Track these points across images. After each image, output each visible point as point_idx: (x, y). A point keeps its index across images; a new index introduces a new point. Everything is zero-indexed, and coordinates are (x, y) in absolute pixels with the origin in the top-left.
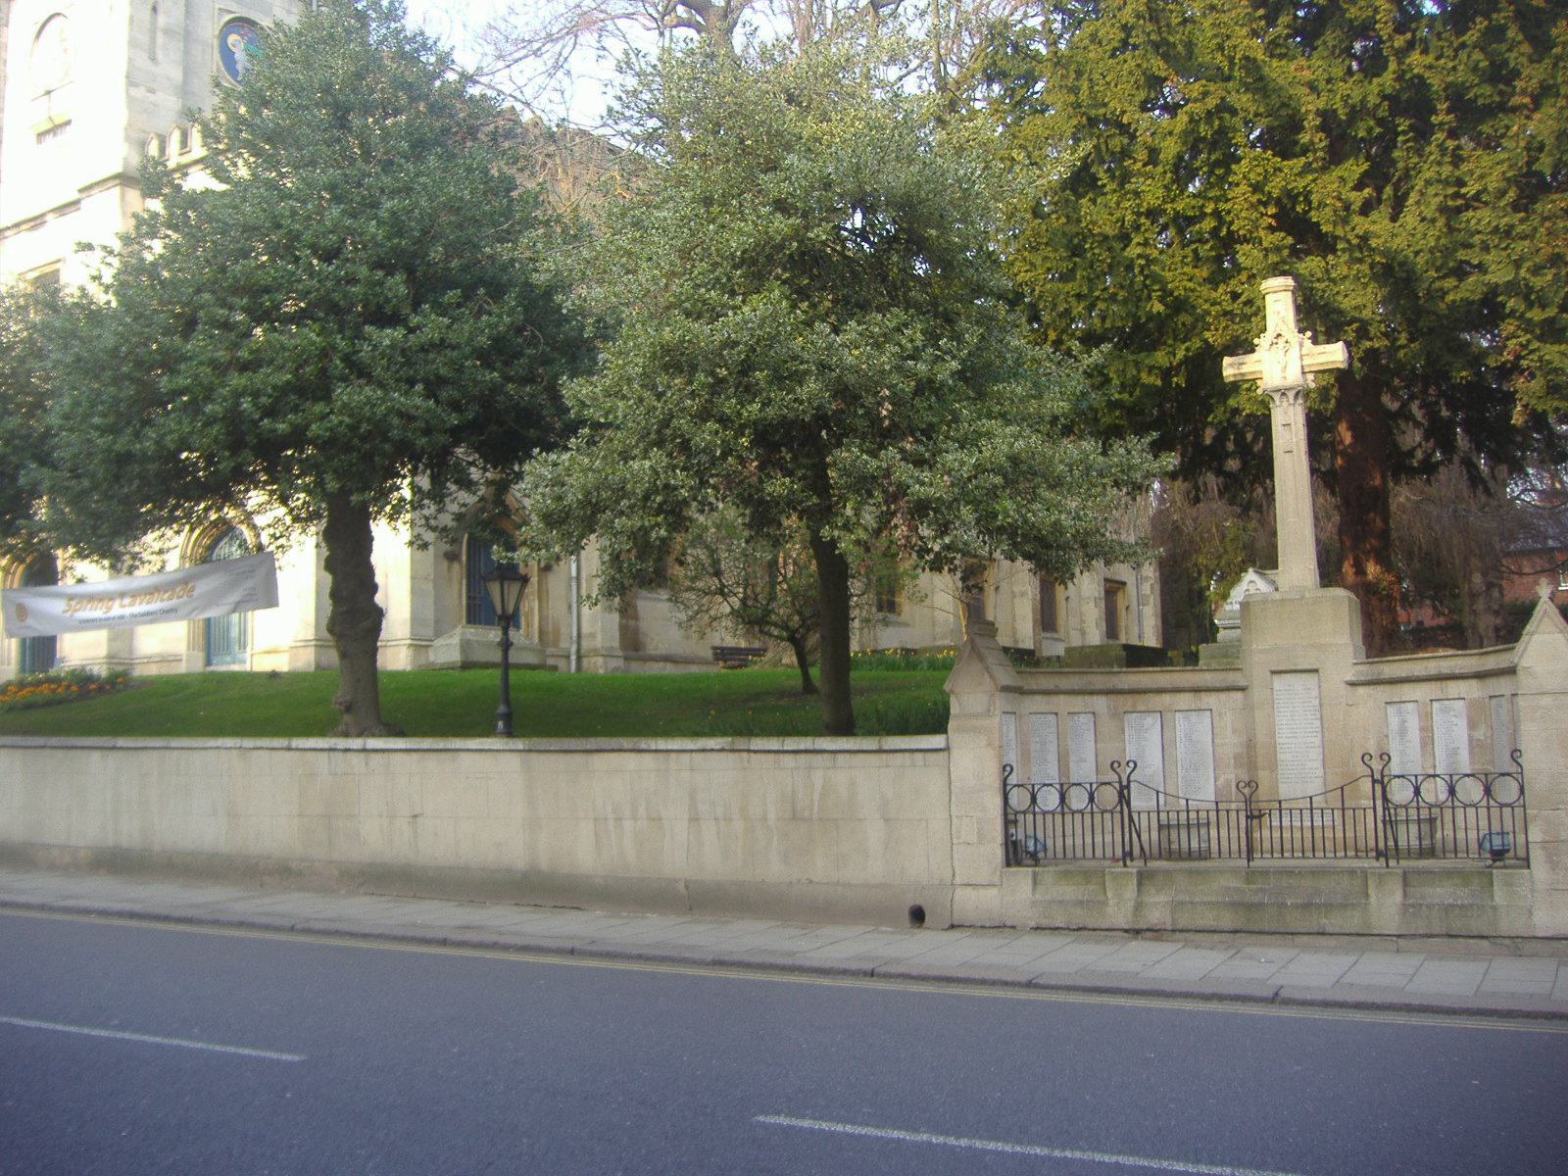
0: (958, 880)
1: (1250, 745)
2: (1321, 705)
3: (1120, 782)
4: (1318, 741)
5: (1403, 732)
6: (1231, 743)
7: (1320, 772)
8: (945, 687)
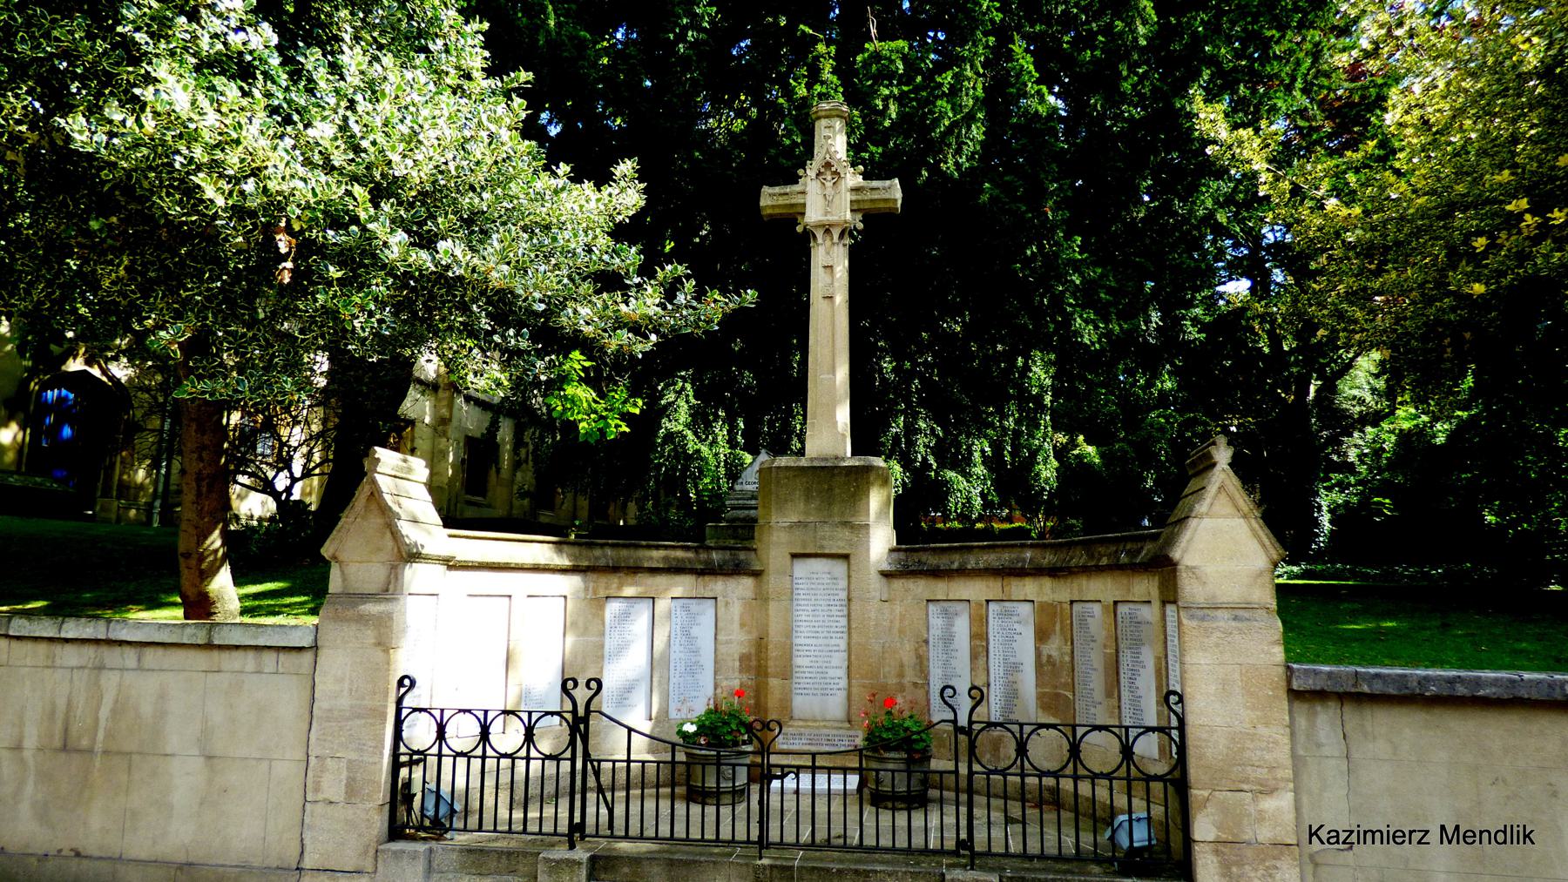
0: (308, 863)
1: (761, 644)
2: (849, 600)
3: (574, 711)
4: (843, 644)
5: (948, 639)
6: (738, 641)
7: (843, 683)
8: (323, 551)
